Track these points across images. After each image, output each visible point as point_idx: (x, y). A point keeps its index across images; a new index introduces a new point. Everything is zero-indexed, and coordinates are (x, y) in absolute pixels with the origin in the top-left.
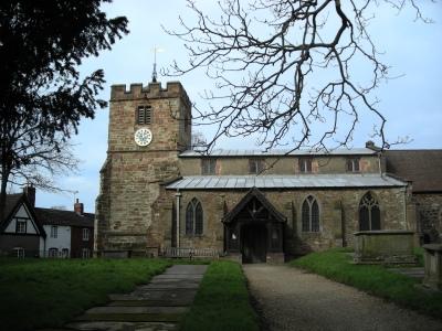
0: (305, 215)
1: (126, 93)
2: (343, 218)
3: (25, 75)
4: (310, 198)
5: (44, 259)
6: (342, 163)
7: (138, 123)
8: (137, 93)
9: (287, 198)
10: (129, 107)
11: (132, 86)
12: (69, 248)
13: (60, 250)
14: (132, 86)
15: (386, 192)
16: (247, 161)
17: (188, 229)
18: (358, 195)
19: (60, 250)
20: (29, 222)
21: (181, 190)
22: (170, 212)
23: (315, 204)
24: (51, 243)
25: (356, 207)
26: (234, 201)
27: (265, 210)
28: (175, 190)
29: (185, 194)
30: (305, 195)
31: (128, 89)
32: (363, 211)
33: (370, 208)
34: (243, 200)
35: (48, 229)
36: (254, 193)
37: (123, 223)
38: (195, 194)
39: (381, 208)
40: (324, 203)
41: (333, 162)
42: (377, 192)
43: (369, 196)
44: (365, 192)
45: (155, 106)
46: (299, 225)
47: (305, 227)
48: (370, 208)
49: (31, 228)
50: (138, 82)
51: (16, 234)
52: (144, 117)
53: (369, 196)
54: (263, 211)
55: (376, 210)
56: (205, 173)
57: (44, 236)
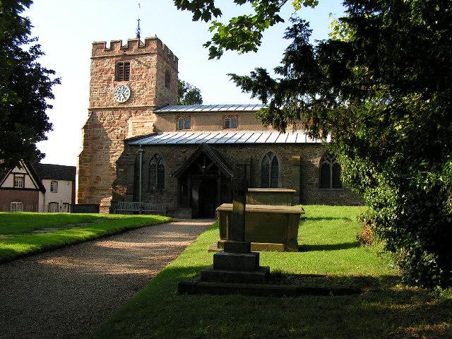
1: (106, 50)
2: (301, 175)
3: (428, 101)
7: (118, 79)
8: (117, 48)
10: (110, 65)
14: (113, 43)
20: (27, 176)
21: (144, 146)
22: (132, 169)
24: (50, 197)
26: (181, 157)
27: (214, 166)
28: (138, 145)
29: (148, 150)
31: (108, 46)
33: (331, 165)
34: (193, 155)
35: (47, 183)
38: (157, 150)
40: (285, 160)
41: (213, 118)
48: (331, 165)
49: (29, 183)
50: (118, 39)
51: (14, 189)
52: (122, 73)
54: (211, 168)
56: (179, 129)
57: (44, 191)
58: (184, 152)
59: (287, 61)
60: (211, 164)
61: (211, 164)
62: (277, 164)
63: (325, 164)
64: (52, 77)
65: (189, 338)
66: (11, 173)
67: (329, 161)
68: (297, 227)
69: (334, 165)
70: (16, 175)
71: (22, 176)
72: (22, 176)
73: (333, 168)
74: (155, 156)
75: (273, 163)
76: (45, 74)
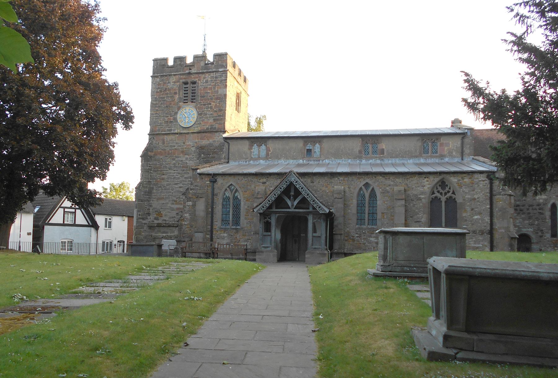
0: (360, 205)
4: (367, 185)
5: (13, 251)
6: (416, 144)
9: (338, 186)
10: (173, 83)
11: (176, 59)
12: (125, 240)
13: (115, 242)
15: (467, 180)
16: (301, 144)
17: (225, 221)
18: (427, 184)
19: (115, 242)
23: (373, 194)
25: (425, 199)
30: (360, 183)
32: (434, 202)
33: (443, 199)
35: (100, 220)
36: (293, 179)
37: (163, 213)
39: (459, 200)
40: (384, 192)
42: (454, 180)
43: (443, 184)
44: (437, 179)
45: (532, 151)
46: (353, 219)
47: (360, 220)
48: (443, 199)
53: (443, 184)
55: (451, 202)
58: (264, 183)
59: (206, 56)
60: (299, 198)
61: (299, 198)
62: (375, 196)
63: (436, 197)
64: (484, 89)
65: (431, 377)
66: (60, 207)
67: (441, 194)
68: (281, 236)
69: (447, 199)
70: (66, 210)
71: (73, 210)
72: (73, 210)
73: (446, 202)
74: (229, 187)
75: (370, 196)
76: (532, 77)
